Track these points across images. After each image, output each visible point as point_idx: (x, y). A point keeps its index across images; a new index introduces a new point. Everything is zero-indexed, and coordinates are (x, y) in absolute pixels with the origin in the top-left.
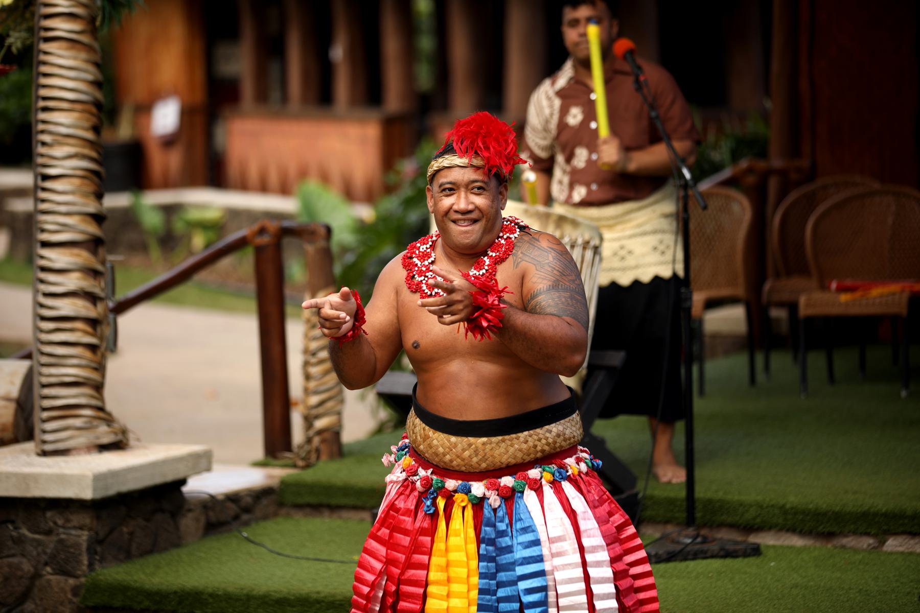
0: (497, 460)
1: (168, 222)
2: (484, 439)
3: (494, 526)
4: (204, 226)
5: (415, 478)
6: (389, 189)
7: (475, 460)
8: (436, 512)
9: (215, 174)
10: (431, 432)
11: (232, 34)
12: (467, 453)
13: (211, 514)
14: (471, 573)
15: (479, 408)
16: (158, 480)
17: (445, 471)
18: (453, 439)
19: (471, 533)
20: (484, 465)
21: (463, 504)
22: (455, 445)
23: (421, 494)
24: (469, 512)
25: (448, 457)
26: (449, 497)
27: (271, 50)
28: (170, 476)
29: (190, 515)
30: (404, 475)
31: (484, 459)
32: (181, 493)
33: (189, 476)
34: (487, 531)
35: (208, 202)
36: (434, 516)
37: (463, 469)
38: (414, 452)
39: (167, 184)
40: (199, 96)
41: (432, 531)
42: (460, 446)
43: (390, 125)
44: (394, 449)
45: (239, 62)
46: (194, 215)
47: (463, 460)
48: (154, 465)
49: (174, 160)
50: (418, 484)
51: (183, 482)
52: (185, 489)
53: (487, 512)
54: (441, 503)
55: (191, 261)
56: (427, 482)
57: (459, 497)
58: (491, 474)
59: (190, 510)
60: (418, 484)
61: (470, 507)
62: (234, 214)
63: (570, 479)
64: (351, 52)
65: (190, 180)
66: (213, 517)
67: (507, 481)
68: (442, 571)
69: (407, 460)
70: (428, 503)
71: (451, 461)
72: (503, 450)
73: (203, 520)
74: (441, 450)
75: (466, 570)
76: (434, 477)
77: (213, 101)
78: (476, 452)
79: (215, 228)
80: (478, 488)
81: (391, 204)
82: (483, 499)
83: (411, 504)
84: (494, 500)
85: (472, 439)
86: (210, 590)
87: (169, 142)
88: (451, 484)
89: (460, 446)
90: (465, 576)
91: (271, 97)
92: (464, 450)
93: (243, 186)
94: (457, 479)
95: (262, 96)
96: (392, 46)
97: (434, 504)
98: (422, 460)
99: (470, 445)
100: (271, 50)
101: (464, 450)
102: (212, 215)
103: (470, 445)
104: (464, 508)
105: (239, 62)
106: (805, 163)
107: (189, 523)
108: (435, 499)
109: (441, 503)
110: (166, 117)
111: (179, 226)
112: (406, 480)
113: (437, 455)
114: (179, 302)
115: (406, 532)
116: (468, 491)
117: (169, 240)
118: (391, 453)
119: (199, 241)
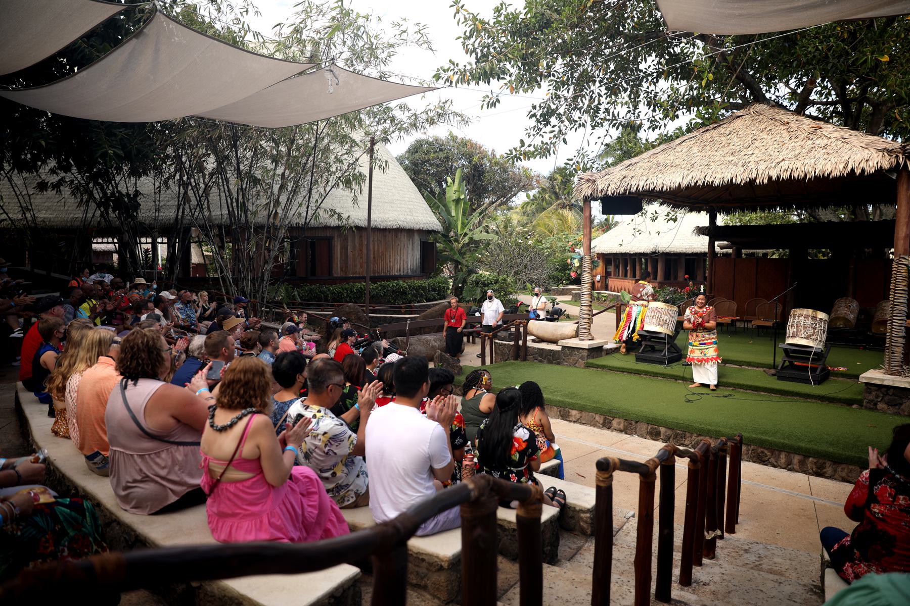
9: (606, 288)
27: (617, 267)
45: (611, 269)
91: (617, 276)
96: (637, 268)
100: (617, 267)
105: (611, 269)
107: (603, 353)
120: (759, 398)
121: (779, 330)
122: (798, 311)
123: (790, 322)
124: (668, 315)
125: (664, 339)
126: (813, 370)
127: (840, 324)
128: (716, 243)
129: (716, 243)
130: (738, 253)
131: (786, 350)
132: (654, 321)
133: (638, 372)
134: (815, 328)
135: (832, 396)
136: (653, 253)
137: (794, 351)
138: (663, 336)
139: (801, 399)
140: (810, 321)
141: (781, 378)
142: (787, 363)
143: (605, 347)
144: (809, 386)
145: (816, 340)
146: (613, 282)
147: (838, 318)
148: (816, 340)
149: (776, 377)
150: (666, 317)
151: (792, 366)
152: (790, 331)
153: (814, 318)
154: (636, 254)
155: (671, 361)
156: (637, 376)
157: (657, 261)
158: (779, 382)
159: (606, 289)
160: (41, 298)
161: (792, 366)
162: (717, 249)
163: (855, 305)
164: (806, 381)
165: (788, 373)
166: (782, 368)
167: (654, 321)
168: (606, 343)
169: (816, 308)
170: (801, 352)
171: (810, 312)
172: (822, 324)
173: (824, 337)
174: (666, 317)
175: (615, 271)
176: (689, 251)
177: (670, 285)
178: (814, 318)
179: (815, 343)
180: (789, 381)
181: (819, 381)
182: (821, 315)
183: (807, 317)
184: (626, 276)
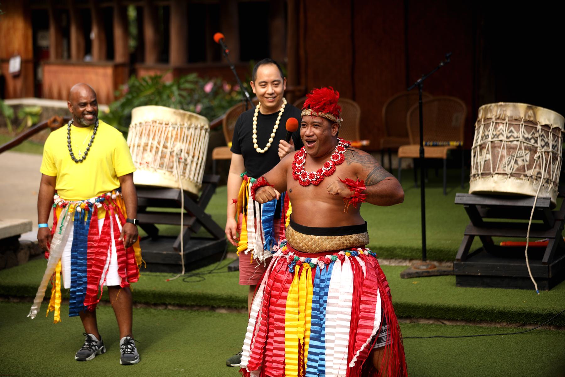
0: (324, 247)
1: (15, 113)
2: (318, 237)
3: (320, 278)
4: (32, 115)
5: (287, 256)
6: (116, 99)
7: (314, 246)
8: (294, 272)
9: (38, 92)
10: (295, 232)
11: (46, 28)
12: (310, 243)
13: (32, 251)
14: (308, 301)
15: (318, 222)
16: (7, 235)
17: (300, 253)
18: (304, 236)
19: (310, 281)
20: (318, 249)
21: (307, 268)
22: (305, 239)
23: (289, 264)
24: (310, 272)
25: (301, 245)
26: (301, 265)
27: (64, 34)
28: (13, 234)
29: (22, 251)
30: (282, 254)
31: (318, 246)
32: (18, 241)
33: (22, 233)
34: (317, 281)
35: (34, 104)
36: (293, 274)
37: (308, 251)
38: (287, 244)
39: (15, 97)
40: (30, 56)
41: (290, 282)
42: (307, 240)
43: (116, 67)
44: (279, 243)
45: (49, 40)
46: (28, 110)
47: (308, 246)
48: (5, 229)
49: (19, 83)
50: (288, 259)
51: (19, 236)
52: (20, 239)
53: (318, 272)
54: (297, 268)
55: (27, 131)
56: (292, 258)
57: (305, 265)
58: (321, 254)
59: (22, 249)
60: (288, 259)
61: (310, 269)
62: (46, 109)
63: (359, 256)
64: (99, 36)
65: (25, 94)
66: (33, 252)
67: (329, 256)
68: (295, 301)
69: (285, 248)
70: (291, 267)
71: (303, 247)
72: (327, 243)
73: (28, 253)
74: (298, 241)
75: (305, 300)
76: (295, 256)
77: (37, 57)
78: (315, 242)
79: (38, 115)
80: (314, 261)
81: (117, 105)
82: (316, 265)
83: (284, 269)
84: (322, 265)
85: (313, 236)
86: (31, 286)
87: (16, 76)
88: (302, 259)
89: (307, 240)
90: (304, 302)
91: (65, 58)
92: (309, 241)
93: (51, 97)
94: (305, 257)
95: (59, 55)
96: (118, 32)
97: (294, 268)
98: (291, 249)
99: (312, 239)
100: (64, 34)
101: (309, 241)
102: (35, 110)
103: (312, 239)
104: (307, 270)
105: (49, 40)
106: (302, 88)
107: (22, 255)
108: (295, 266)
109: (297, 268)
110: (15, 65)
111: (21, 115)
112: (282, 257)
113: (296, 243)
114: (21, 151)
115: (280, 282)
116: (309, 262)
117: (16, 122)
118: (277, 245)
119: (30, 122)
121: (457, 168)
122: (493, 110)
123: (478, 140)
125: (175, 203)
126: (536, 253)
131: (471, 209)
132: (149, 157)
133: (428, 275)
134: (533, 150)
137: (492, 211)
138: (172, 196)
139: (512, 328)
140: (521, 133)
141: (464, 280)
142: (477, 244)
144: (530, 292)
145: (538, 177)
148: (538, 178)
149: (453, 279)
150: (179, 145)
151: (490, 249)
152: (479, 159)
153: (531, 124)
155: (196, 262)
158: (461, 290)
160: (534, 278)
161: (490, 249)
164: (520, 282)
165: (478, 267)
166: (467, 256)
167: (149, 157)
169: (535, 100)
170: (507, 208)
171: (521, 109)
172: (550, 139)
173: (556, 170)
174: (179, 145)
175: (58, 45)
177: (205, 75)
178: (531, 124)
180: (508, 286)
182: (547, 117)
183: (514, 122)
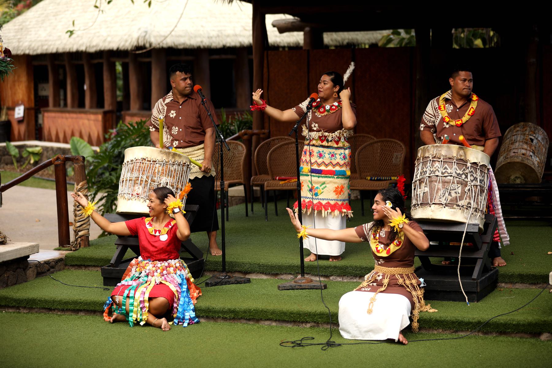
27: (60, 85)
45: (48, 90)
91: (60, 104)
96: (107, 84)
100: (60, 85)
105: (48, 90)
107: (30, 272)
120: (433, 337)
123: (417, 175)
124: (169, 174)
127: (516, 178)
128: (270, 19)
129: (270, 19)
130: (314, 39)
135: (503, 319)
136: (138, 48)
139: (447, 335)
140: (454, 169)
143: (35, 258)
144: (461, 304)
145: (468, 207)
146: (52, 120)
147: (511, 165)
148: (468, 207)
153: (462, 162)
154: (102, 54)
156: (250, 326)
157: (149, 65)
159: (39, 137)
162: (274, 36)
163: (540, 137)
168: (35, 249)
176: (217, 42)
178: (462, 162)
179: (465, 217)
181: (478, 294)
183: (448, 160)
184: (81, 104)
